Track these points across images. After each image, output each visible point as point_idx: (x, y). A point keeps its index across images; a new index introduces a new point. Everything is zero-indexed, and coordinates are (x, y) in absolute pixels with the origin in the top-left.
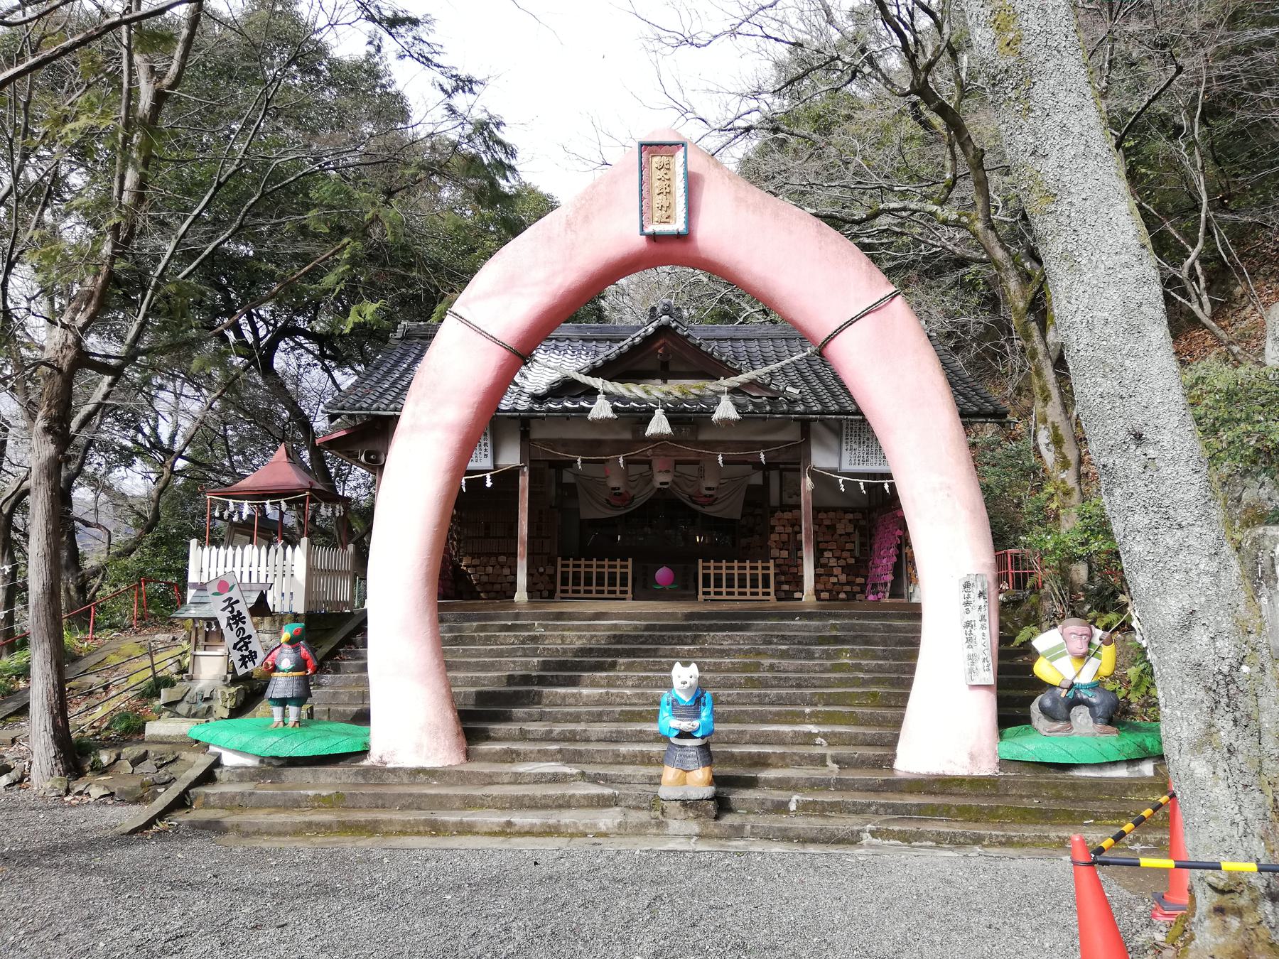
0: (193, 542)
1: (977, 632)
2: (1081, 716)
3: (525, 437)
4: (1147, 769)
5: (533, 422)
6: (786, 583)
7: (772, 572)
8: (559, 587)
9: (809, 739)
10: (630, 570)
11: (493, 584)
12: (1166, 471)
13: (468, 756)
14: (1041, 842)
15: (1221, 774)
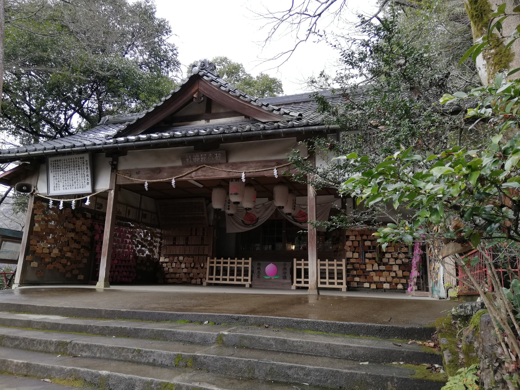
6: (358, 276)
10: (250, 266)
11: (176, 273)
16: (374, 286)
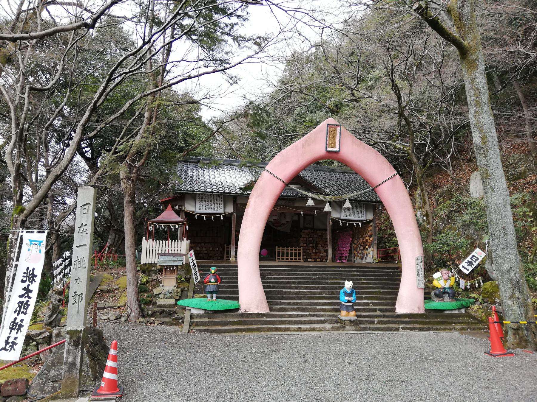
0: (144, 238)
1: (420, 273)
2: (446, 298)
3: (235, 202)
4: (463, 311)
5: (238, 198)
7: (302, 251)
8: (225, 256)
9: (368, 304)
12: (509, 236)
13: (271, 309)
14: (445, 329)
15: (515, 303)
16: (313, 260)
